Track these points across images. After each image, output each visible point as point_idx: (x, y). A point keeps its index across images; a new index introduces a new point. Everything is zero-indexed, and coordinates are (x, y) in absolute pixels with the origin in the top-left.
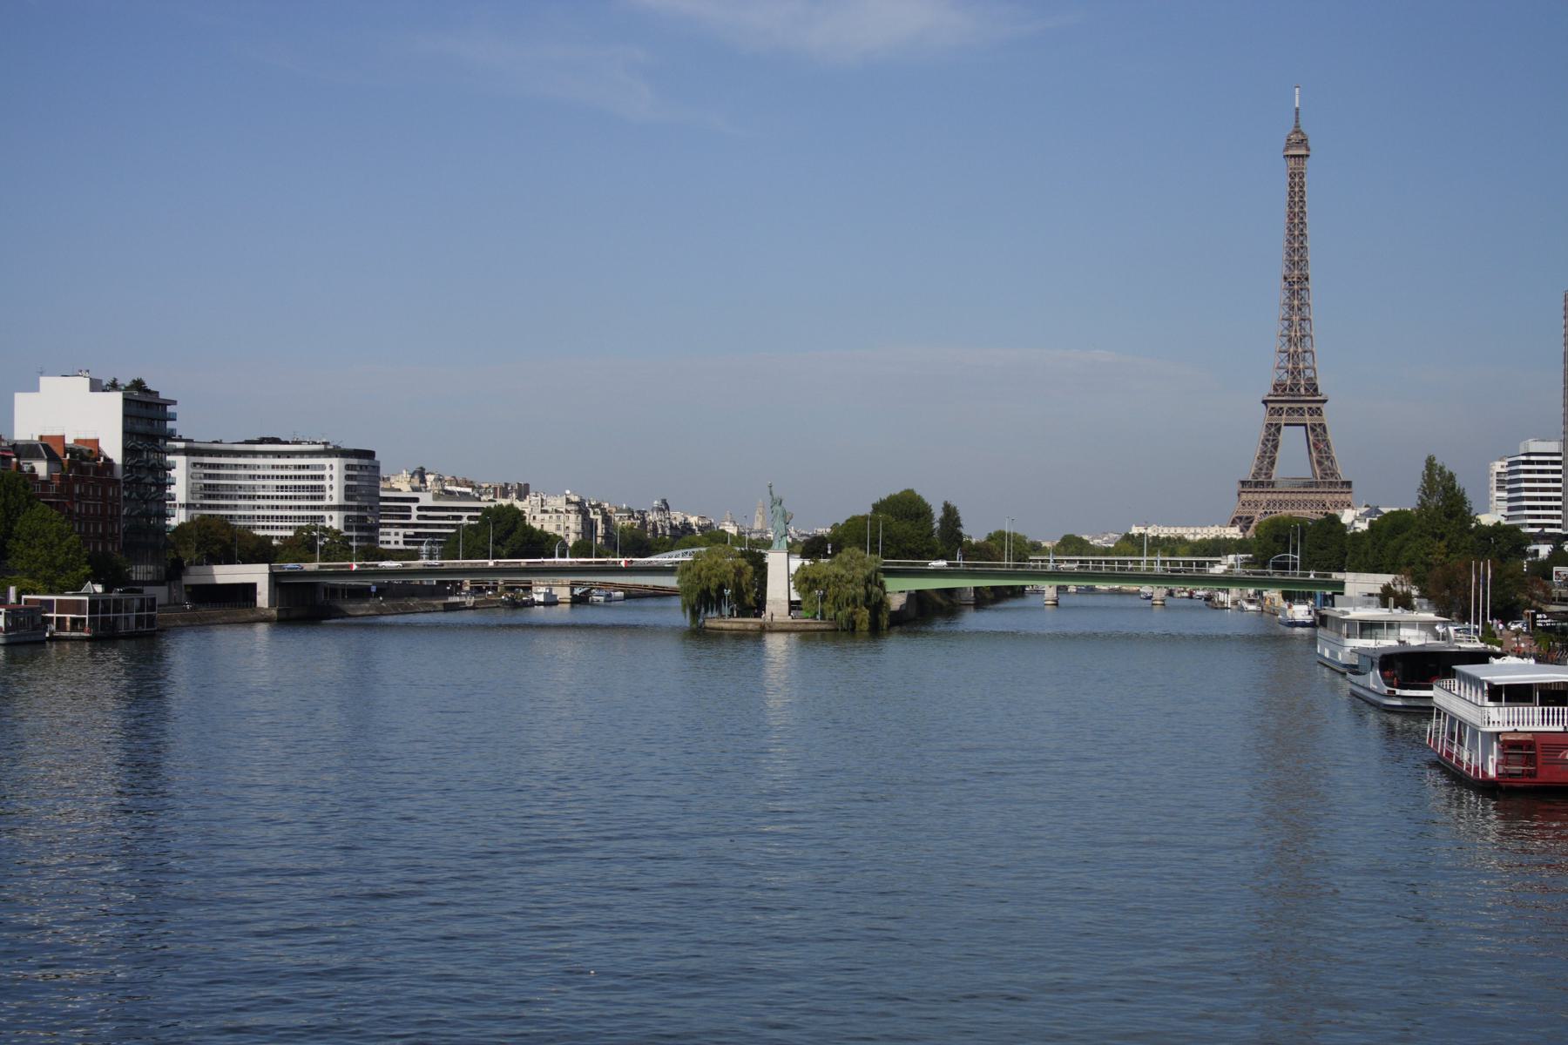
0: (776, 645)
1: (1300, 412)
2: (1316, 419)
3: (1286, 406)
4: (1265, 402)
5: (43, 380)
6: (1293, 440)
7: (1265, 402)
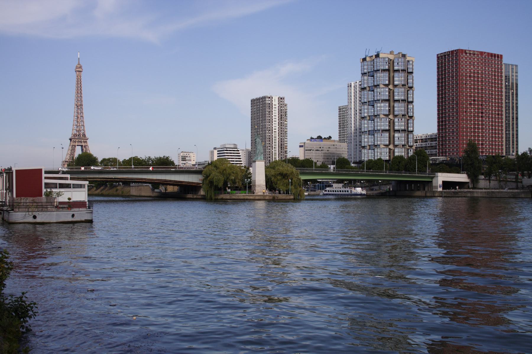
2: (85, 144)
3: (77, 140)
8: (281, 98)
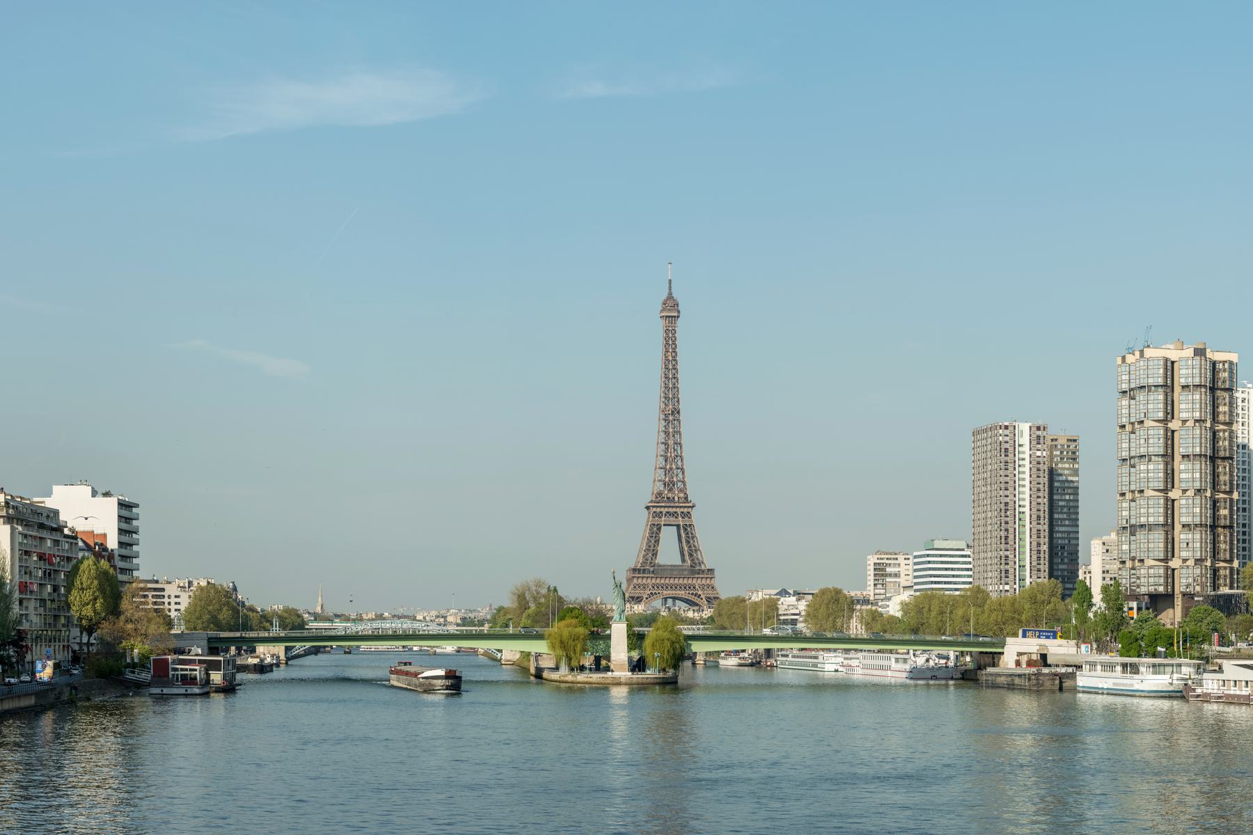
0: (619, 694)
1: (675, 515)
3: (664, 510)
4: (648, 508)
5: (56, 488)
6: (669, 536)
7: (648, 508)
8: (1038, 428)
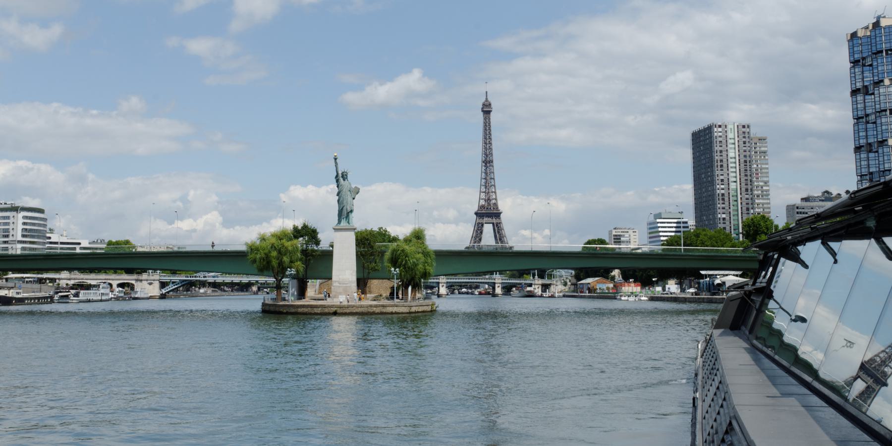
2: (497, 221)
6: (488, 229)
